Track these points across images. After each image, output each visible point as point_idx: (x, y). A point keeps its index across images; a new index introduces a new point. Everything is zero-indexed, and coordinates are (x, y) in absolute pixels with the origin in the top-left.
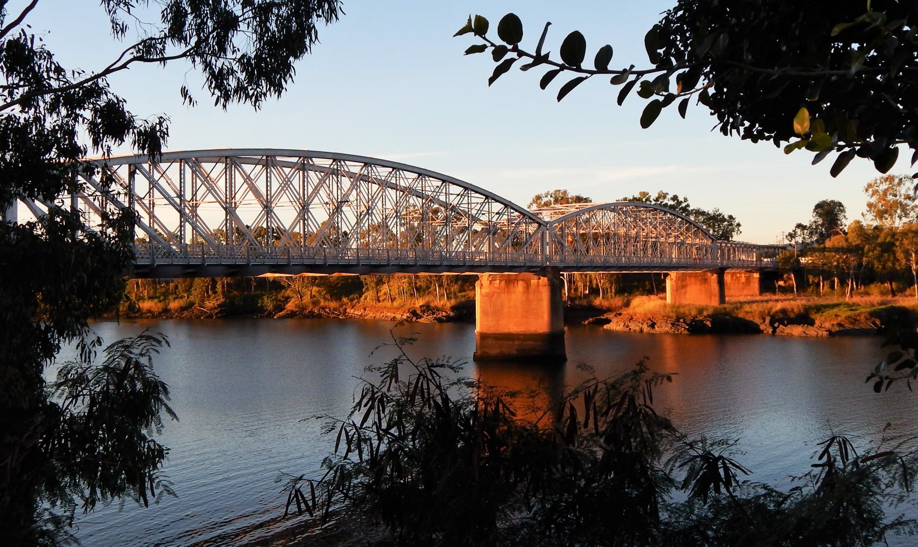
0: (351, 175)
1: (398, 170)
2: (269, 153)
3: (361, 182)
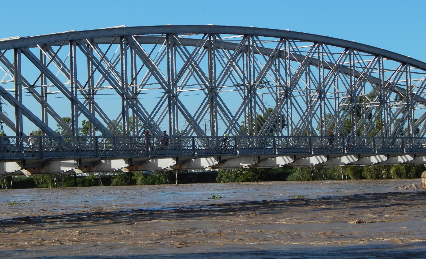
0: (265, 52)
1: (321, 43)
2: (169, 30)
3: (281, 59)
